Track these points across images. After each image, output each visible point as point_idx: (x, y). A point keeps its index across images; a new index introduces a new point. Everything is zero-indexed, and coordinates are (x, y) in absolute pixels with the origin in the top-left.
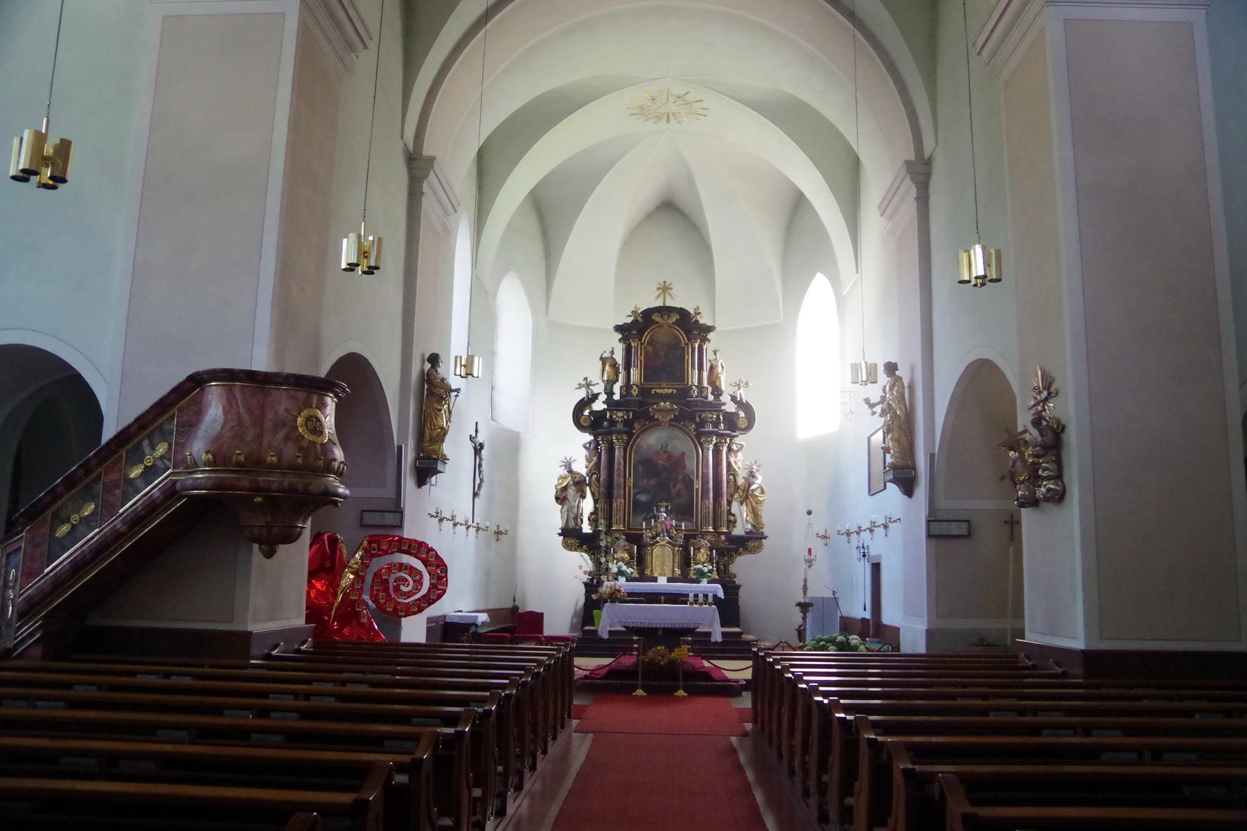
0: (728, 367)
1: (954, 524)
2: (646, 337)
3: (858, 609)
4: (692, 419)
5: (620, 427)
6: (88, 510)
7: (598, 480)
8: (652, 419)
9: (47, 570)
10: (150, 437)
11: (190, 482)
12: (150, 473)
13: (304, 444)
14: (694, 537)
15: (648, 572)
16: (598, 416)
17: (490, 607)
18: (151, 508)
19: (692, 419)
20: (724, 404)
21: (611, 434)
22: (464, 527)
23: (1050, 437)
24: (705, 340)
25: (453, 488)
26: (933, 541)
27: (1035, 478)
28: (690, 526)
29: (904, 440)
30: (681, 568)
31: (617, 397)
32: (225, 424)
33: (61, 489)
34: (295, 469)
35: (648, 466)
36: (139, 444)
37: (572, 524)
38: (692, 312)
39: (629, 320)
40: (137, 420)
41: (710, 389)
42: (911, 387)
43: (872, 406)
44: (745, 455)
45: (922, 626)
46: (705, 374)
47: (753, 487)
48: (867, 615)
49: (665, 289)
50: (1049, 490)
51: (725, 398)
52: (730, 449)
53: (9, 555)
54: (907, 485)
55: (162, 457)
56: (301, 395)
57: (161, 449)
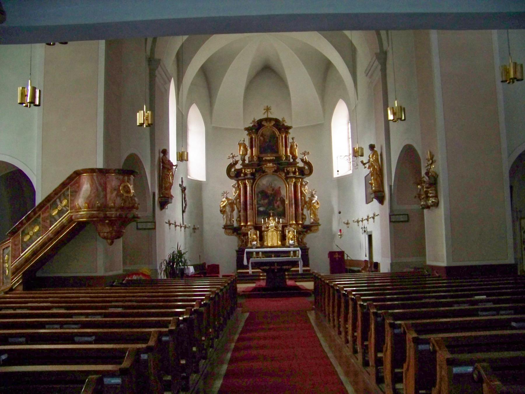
0: (300, 147)
1: (401, 216)
2: (260, 131)
3: (364, 257)
4: (283, 170)
5: (249, 176)
6: (36, 229)
7: (240, 202)
8: (264, 172)
9: (21, 255)
10: (59, 198)
11: (79, 216)
12: (61, 213)
13: (124, 197)
14: (286, 226)
15: (265, 244)
16: (238, 173)
17: (193, 264)
18: (63, 227)
19: (283, 171)
20: (298, 163)
21: (245, 179)
22: (174, 225)
23: (433, 179)
24: (287, 133)
25: (175, 211)
26: (393, 224)
27: (427, 197)
28: (284, 221)
29: (379, 179)
30: (281, 242)
31: (247, 162)
32: (91, 191)
33: (25, 221)
34: (122, 208)
35: (264, 194)
36: (55, 201)
37: (229, 223)
38: (281, 120)
39: (251, 125)
40: (54, 191)
41: (291, 156)
42: (381, 155)
43: (364, 164)
44: (309, 186)
45: (389, 261)
46: (288, 149)
47: (313, 202)
48: (367, 259)
49: (268, 109)
50: (433, 202)
51: (298, 160)
52: (301, 184)
53: (4, 249)
54: (381, 201)
55: (65, 206)
56: (121, 177)
57: (65, 202)
